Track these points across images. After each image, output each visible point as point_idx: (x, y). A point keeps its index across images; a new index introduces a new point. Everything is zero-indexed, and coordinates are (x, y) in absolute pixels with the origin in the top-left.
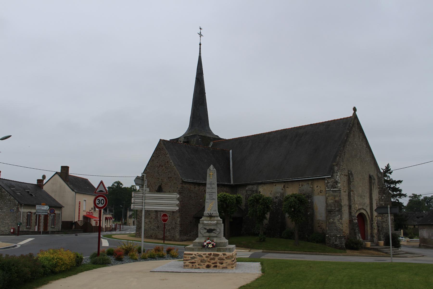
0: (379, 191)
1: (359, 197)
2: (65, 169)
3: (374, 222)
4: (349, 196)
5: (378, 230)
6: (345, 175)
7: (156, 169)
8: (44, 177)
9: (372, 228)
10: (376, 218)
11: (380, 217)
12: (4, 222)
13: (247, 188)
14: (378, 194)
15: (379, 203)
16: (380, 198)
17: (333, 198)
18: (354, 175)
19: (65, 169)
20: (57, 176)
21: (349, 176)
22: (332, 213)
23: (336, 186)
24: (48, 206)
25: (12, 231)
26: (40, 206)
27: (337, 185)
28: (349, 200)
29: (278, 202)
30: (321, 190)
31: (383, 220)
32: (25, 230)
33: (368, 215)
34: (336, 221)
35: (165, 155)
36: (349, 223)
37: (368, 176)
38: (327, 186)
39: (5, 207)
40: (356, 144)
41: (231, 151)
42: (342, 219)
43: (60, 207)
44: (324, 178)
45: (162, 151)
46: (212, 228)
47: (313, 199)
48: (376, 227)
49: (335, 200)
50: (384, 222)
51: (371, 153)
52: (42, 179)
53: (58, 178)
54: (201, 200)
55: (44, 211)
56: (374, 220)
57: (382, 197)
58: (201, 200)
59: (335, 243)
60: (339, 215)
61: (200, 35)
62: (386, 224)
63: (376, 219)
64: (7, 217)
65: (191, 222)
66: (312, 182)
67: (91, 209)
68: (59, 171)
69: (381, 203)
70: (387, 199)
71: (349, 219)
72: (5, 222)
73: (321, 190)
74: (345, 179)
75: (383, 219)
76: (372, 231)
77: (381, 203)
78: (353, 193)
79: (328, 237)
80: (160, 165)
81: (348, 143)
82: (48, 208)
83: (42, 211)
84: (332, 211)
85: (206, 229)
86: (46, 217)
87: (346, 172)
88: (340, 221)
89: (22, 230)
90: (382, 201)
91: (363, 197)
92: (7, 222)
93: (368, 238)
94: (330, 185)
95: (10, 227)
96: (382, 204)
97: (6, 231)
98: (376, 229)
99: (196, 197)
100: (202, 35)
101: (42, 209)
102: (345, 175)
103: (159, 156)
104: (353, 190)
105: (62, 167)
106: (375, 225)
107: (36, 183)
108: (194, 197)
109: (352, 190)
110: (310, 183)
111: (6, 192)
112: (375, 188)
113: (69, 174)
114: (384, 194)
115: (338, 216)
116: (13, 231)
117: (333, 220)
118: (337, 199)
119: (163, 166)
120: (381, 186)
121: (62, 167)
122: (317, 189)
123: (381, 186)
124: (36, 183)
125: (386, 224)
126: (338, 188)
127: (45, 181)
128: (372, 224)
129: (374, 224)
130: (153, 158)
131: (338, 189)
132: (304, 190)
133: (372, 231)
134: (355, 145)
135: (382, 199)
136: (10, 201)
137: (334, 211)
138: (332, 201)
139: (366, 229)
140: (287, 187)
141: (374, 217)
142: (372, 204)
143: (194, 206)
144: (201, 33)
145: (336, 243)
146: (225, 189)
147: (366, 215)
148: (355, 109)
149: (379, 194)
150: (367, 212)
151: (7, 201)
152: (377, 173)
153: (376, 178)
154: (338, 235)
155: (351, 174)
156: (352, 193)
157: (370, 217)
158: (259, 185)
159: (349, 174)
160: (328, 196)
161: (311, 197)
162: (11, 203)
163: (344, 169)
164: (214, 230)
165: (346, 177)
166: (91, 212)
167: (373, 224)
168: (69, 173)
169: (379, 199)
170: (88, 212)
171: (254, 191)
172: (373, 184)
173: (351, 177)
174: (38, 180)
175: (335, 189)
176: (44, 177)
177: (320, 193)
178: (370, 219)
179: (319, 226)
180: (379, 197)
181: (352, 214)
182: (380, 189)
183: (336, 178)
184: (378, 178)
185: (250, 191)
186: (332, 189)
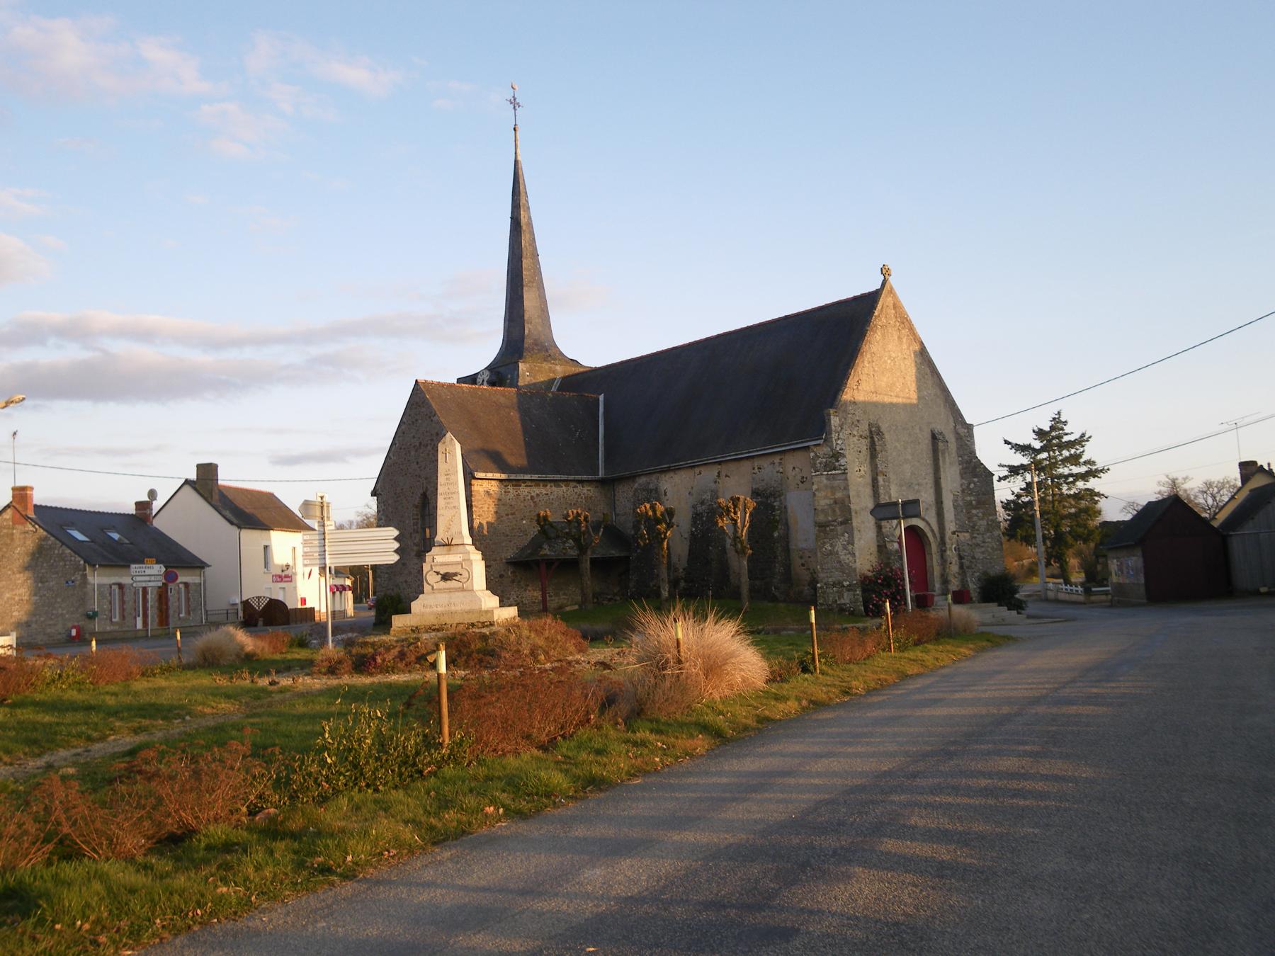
0: (963, 469)
1: (904, 488)
2: (207, 472)
3: (948, 546)
4: (873, 486)
5: (961, 566)
6: (861, 436)
7: (413, 453)
8: (152, 494)
9: (944, 561)
10: (955, 536)
11: (967, 535)
12: (52, 614)
13: (636, 485)
14: (958, 477)
15: (963, 499)
16: (964, 487)
17: (829, 494)
18: (887, 436)
19: (207, 472)
20: (187, 488)
21: (872, 438)
22: (828, 529)
23: (837, 464)
24: (162, 566)
25: (74, 632)
26: (141, 565)
27: (838, 461)
28: (874, 496)
29: (708, 513)
30: (803, 478)
31: (974, 541)
32: (108, 628)
33: (932, 531)
34: (839, 548)
35: (430, 417)
36: (878, 551)
37: (929, 436)
38: (814, 465)
39: (54, 576)
40: (890, 357)
41: (601, 397)
42: (853, 544)
43: (197, 564)
44: (808, 447)
45: (423, 410)
46: (451, 570)
47: (785, 499)
48: (955, 560)
49: (835, 498)
50: (978, 545)
51: (936, 376)
52: (148, 500)
53: (190, 494)
54: (524, 522)
55: (153, 578)
56: (947, 540)
57: (969, 484)
58: (524, 522)
59: (838, 602)
60: (846, 535)
61: (515, 103)
62: (983, 549)
63: (954, 540)
64: (59, 600)
65: (501, 576)
66: (781, 459)
67: (285, 568)
68: (193, 476)
69: (969, 498)
70: (983, 490)
71: (878, 541)
72: (54, 612)
73: (803, 478)
74: (864, 445)
75: (976, 537)
76: (944, 569)
77: (969, 498)
78: (884, 480)
79: (821, 588)
80: (420, 443)
81: (868, 356)
82: (163, 569)
83: (148, 578)
84: (828, 526)
85: (438, 573)
86: (163, 594)
87: (864, 427)
88: (850, 547)
89: (101, 629)
90: (970, 495)
91: (917, 487)
92: (60, 611)
93: (934, 586)
94: (820, 463)
95: (70, 625)
96: (971, 501)
97: (60, 634)
98: (954, 562)
99: (512, 514)
100: (511, 103)
101: (146, 573)
102: (861, 436)
103: (417, 420)
104: (885, 470)
105: (200, 467)
106: (951, 554)
107: (132, 510)
108: (507, 515)
109: (881, 472)
110: (777, 460)
111: (52, 538)
112: (948, 464)
113: (220, 482)
114: (976, 476)
115: (844, 536)
116: (78, 632)
117: (831, 545)
118: (839, 495)
119: (427, 445)
120: (966, 457)
121: (200, 467)
122: (794, 474)
123: (966, 457)
124: (134, 513)
125: (983, 549)
126: (840, 469)
127: (157, 505)
128: (942, 552)
129: (948, 552)
130: (403, 427)
131: (840, 472)
132: (763, 480)
133: (944, 569)
134: (889, 361)
135: (970, 489)
136: (65, 561)
137: (832, 525)
138: (828, 502)
139: (928, 564)
140: (726, 476)
141: (948, 534)
142: (942, 502)
143: (507, 536)
144: (515, 99)
145: (842, 601)
146: (585, 491)
147: (927, 530)
148: (885, 271)
149: (962, 478)
150: (928, 523)
151: (55, 561)
152: (955, 427)
153: (951, 438)
154: (846, 581)
155: (879, 433)
156: (880, 479)
157: (938, 535)
158: (663, 476)
159: (871, 432)
160: (817, 490)
161: (780, 496)
162: (65, 565)
163: (858, 421)
164: (456, 574)
165: (863, 441)
166: (283, 574)
167: (945, 551)
168: (219, 478)
169: (963, 491)
170: (276, 576)
171: (651, 490)
172: (943, 453)
173: (876, 439)
174: (138, 504)
175: (834, 472)
176: (152, 494)
177: (800, 484)
178: (939, 540)
179: (803, 565)
180: (961, 485)
181: (884, 530)
182: (965, 465)
183: (837, 444)
184: (957, 439)
185: (644, 490)
186: (826, 473)
